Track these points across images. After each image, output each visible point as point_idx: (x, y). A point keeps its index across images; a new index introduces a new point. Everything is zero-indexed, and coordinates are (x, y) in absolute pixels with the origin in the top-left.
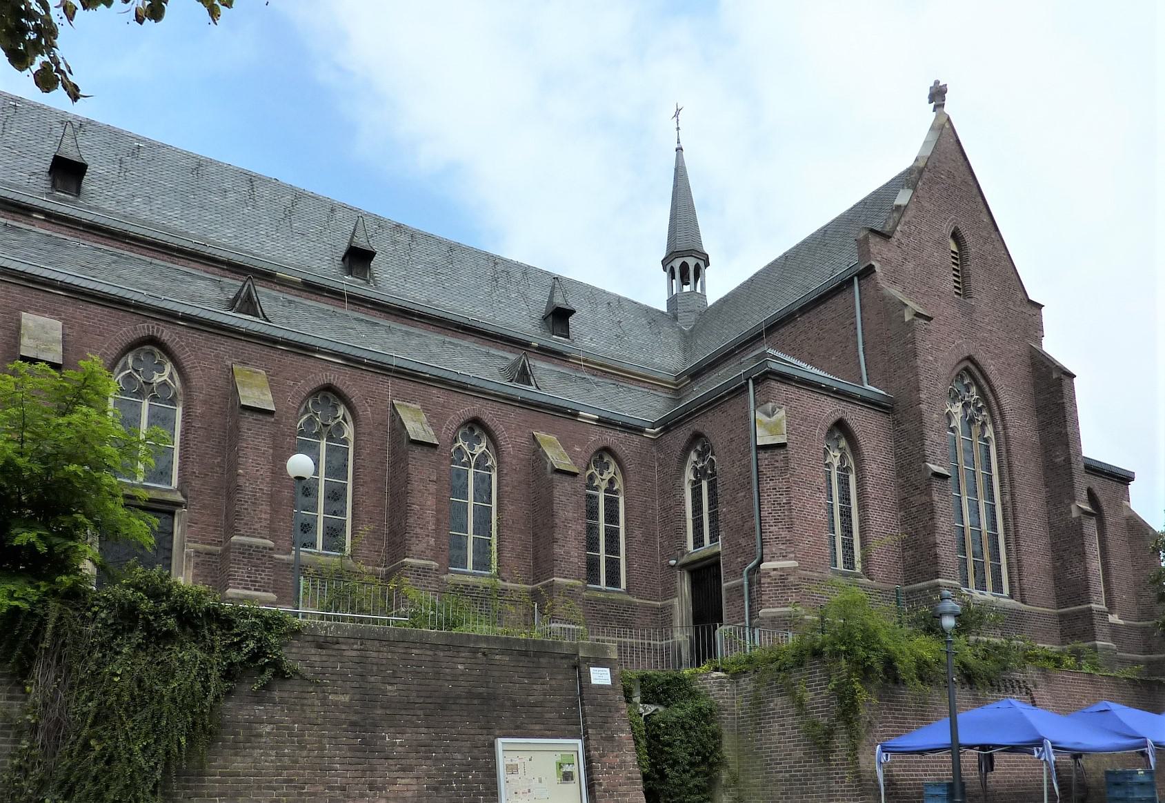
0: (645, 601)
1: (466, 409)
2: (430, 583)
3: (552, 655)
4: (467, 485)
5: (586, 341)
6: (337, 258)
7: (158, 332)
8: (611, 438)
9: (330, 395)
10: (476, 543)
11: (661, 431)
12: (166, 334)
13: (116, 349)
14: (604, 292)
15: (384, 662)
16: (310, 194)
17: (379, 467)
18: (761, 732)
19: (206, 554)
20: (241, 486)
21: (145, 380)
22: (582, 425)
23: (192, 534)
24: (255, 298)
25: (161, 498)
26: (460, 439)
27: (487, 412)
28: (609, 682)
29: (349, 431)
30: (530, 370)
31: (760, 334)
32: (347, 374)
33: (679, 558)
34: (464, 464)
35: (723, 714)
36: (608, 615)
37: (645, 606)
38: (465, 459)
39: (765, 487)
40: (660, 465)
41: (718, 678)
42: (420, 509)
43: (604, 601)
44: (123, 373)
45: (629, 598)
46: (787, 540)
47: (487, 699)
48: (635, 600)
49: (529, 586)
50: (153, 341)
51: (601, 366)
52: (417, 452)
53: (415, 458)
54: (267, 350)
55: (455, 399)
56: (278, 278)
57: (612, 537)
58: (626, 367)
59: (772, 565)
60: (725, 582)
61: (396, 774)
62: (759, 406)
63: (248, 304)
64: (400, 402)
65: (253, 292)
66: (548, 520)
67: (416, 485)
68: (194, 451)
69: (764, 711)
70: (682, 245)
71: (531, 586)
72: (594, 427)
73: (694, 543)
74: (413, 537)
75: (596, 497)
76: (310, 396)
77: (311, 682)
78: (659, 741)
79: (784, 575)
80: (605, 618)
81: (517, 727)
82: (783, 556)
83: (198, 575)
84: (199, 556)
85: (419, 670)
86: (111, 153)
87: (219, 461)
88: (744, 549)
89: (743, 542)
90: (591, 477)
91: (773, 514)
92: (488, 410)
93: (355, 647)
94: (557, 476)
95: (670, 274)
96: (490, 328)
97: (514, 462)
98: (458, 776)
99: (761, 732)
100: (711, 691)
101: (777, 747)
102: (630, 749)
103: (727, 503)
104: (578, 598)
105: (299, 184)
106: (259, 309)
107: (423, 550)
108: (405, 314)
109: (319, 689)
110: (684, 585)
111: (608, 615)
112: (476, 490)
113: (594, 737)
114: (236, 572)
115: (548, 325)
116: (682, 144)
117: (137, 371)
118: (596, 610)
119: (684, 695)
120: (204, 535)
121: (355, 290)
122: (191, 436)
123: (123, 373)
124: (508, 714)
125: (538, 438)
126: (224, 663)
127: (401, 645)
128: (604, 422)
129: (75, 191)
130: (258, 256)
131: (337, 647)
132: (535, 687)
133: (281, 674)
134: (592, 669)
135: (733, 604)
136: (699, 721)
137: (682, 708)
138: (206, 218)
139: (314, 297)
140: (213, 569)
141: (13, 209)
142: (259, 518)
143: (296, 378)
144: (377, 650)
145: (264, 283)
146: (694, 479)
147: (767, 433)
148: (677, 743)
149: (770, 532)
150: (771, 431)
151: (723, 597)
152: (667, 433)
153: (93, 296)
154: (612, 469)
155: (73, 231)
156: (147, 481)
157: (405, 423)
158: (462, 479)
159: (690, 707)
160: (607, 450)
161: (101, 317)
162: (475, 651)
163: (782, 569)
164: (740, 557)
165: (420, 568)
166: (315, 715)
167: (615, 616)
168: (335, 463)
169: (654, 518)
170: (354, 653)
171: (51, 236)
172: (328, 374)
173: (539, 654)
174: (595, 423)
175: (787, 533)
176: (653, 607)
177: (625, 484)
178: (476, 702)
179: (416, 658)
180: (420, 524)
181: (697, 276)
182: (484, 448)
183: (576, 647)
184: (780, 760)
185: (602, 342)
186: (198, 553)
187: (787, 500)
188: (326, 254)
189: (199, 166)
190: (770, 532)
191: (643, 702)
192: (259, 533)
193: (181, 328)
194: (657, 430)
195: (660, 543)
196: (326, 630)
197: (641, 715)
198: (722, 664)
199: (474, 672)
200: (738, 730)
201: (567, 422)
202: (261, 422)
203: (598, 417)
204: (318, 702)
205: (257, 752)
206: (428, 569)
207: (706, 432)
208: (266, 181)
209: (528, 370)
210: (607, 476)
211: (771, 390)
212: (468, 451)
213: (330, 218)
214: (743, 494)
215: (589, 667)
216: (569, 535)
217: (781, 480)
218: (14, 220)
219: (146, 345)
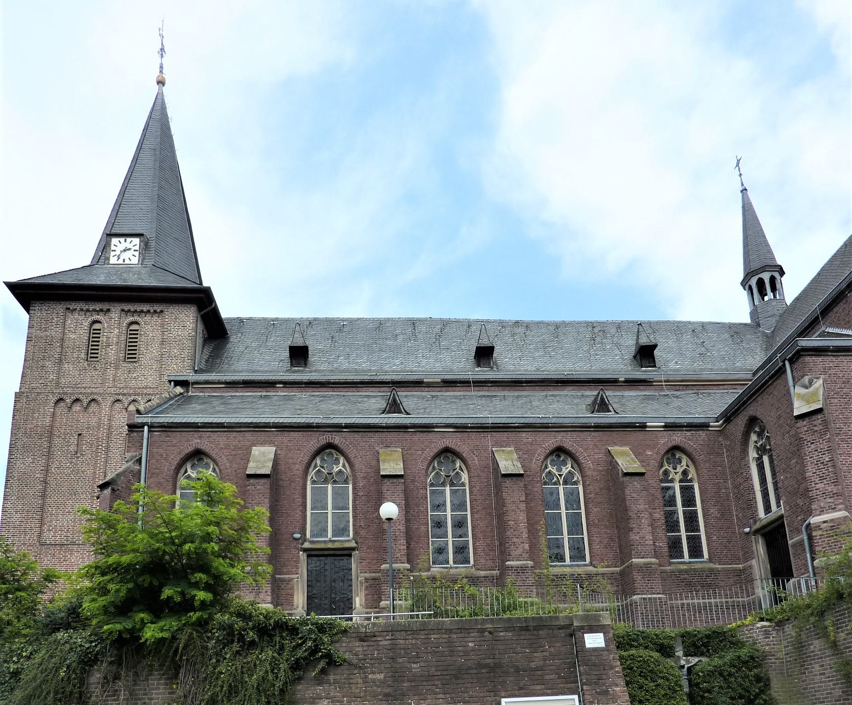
0: (726, 566)
1: (551, 442)
2: (527, 578)
3: (550, 627)
4: (559, 498)
5: (672, 365)
6: (471, 358)
7: (332, 439)
8: (678, 438)
9: (449, 454)
10: (571, 542)
11: (724, 422)
12: (337, 439)
13: (308, 456)
14: (689, 322)
15: (410, 646)
16: (454, 320)
17: (487, 498)
18: (805, 673)
19: (372, 579)
20: (385, 530)
21: (328, 472)
22: (650, 433)
23: (362, 567)
24: (399, 401)
25: (342, 547)
26: (549, 465)
27: (568, 441)
29: (465, 477)
30: (608, 400)
31: (817, 318)
32: (458, 437)
33: (752, 526)
34: (555, 484)
35: (770, 659)
36: (692, 582)
37: (725, 570)
38: (555, 479)
39: (807, 451)
40: (727, 450)
41: (763, 627)
42: (515, 523)
44: (315, 471)
45: (712, 565)
46: (834, 494)
47: (494, 668)
48: (717, 566)
49: (618, 568)
50: (330, 446)
51: (682, 381)
52: (508, 482)
53: (507, 487)
54: (402, 434)
55: (540, 436)
56: (425, 383)
57: (691, 519)
58: (704, 377)
59: (822, 519)
60: (791, 540)
62: (796, 382)
63: (394, 407)
64: (499, 448)
65: (397, 397)
66: (624, 515)
67: (510, 507)
68: (360, 512)
69: (806, 653)
70: (755, 266)
71: (619, 568)
72: (662, 432)
73: (765, 511)
74: (511, 545)
75: (673, 488)
76: (434, 459)
77: (356, 667)
78: (700, 688)
79: (835, 525)
81: (521, 689)
82: (832, 509)
83: (368, 595)
84: (367, 582)
85: (436, 650)
86: (327, 334)
87: (376, 515)
88: (802, 509)
89: (800, 502)
90: (666, 473)
91: (818, 473)
92: (568, 439)
93: (388, 637)
94: (627, 478)
95: (750, 291)
96: (582, 377)
97: (595, 474)
99: (805, 673)
100: (757, 640)
101: (819, 687)
102: (624, 701)
103: (784, 471)
104: (655, 572)
105: (445, 316)
106: (402, 408)
107: (520, 553)
108: (516, 384)
109: (361, 671)
110: (760, 548)
111: (692, 582)
112: (567, 501)
113: (588, 693)
114: (385, 589)
115: (637, 362)
116: (746, 185)
117: (322, 467)
118: (680, 579)
119: (725, 646)
120: (371, 567)
121: (478, 377)
122: (357, 502)
123: (315, 471)
124: (511, 679)
125: (612, 452)
126: (293, 659)
127: (423, 632)
128: (670, 427)
129: (303, 363)
130: (415, 372)
131: (374, 639)
132: (536, 655)
133: (332, 662)
134: (586, 635)
135: (799, 558)
136: (740, 669)
137: (721, 657)
138: (383, 357)
139: (451, 389)
140: (377, 589)
141: (268, 385)
142: (399, 550)
143: (423, 449)
144: (404, 638)
145: (403, 389)
146: (757, 456)
147: (803, 403)
148: (716, 689)
149: (816, 489)
150: (807, 400)
151: (790, 553)
152: (729, 423)
153: (292, 427)
154: (684, 463)
155: (300, 389)
156: (335, 537)
157: (499, 463)
158: (555, 495)
159: (729, 656)
160: (676, 448)
161: (298, 439)
162: (482, 631)
163: (832, 520)
164: (800, 515)
165: (519, 568)
166: (357, 691)
167: (699, 581)
168: (456, 502)
169: (728, 495)
171: (286, 395)
172: (445, 441)
173: (538, 628)
174: (663, 429)
175: (833, 487)
176: (735, 570)
177: (698, 475)
178: (484, 671)
179: (435, 641)
180: (515, 535)
181: (774, 289)
182: (570, 468)
183: (571, 619)
184: (823, 698)
185: (686, 363)
186: (366, 579)
187: (829, 458)
188: (463, 357)
189: (380, 325)
190: (816, 489)
191: (686, 655)
192: (400, 560)
193: (346, 434)
194: (721, 422)
195: (736, 515)
196: (366, 628)
197: (683, 667)
198: (767, 614)
199: (482, 648)
200: (788, 673)
201: (638, 433)
202: (395, 484)
203: (664, 424)
204: (360, 681)
206: (525, 567)
207: (758, 415)
208: (420, 320)
209: (606, 400)
210: (680, 469)
211: (806, 365)
213: (467, 332)
214: (795, 460)
215: (583, 633)
216: (642, 523)
217: (821, 442)
218: (267, 392)
219: (326, 449)
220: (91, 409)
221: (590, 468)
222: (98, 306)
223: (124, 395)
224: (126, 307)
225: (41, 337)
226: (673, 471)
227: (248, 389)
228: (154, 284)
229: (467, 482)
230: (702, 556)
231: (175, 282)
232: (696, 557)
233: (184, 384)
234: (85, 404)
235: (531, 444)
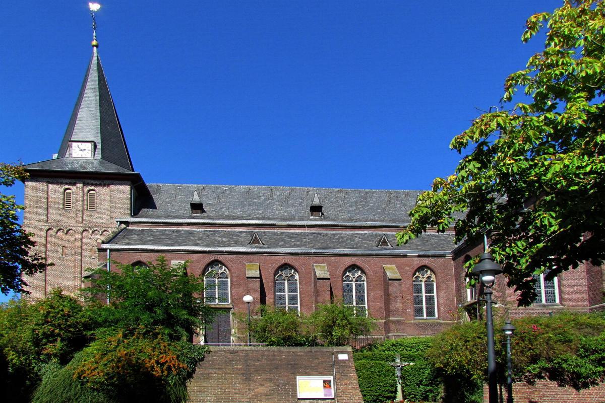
8: (426, 261)
29: (297, 277)
34: (350, 281)
38: (351, 279)
45: (439, 321)
75: (421, 285)
81: (306, 373)
94: (391, 281)
158: (350, 286)
177: (436, 279)
205: (211, 381)
210: (426, 276)
221: (371, 275)
227: (166, 226)
228: (103, 170)
229: (298, 279)
231: (116, 169)
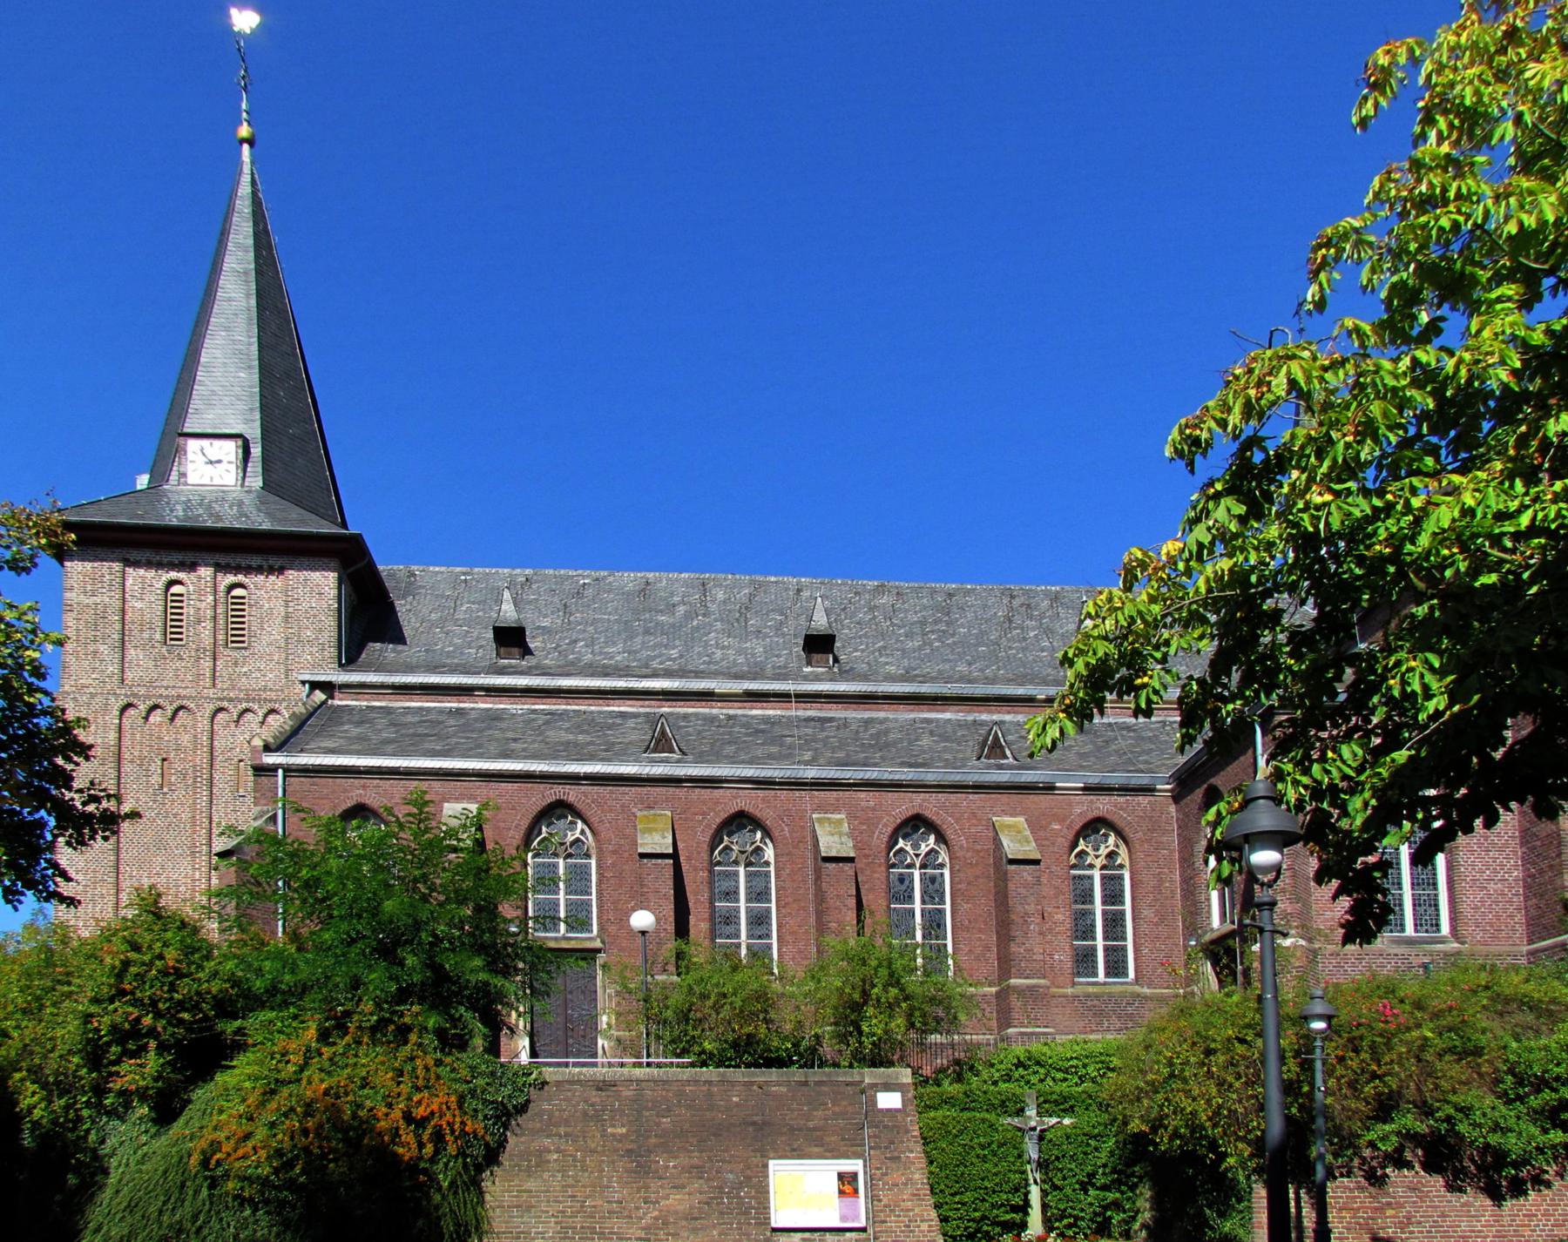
8: (1103, 805)
12: (571, 794)
28: (899, 1105)
29: (769, 853)
43: (1097, 996)
55: (890, 797)
57: (1114, 924)
61: (667, 1191)
75: (1091, 878)
80: (1100, 1014)
81: (794, 1150)
94: (1013, 867)
98: (728, 1193)
125: (997, 825)
158: (907, 882)
170: (631, 1093)
205: (546, 1175)
210: (1103, 851)
212: (911, 852)
220: (178, 721)
221: (961, 847)
222: (176, 557)
223: (230, 700)
224: (223, 560)
225: (88, 606)
226: (1092, 853)
228: (265, 527)
229: (772, 861)
230: (1126, 975)
231: (303, 522)
232: (1116, 975)
233: (327, 687)
234: (169, 713)
235: (874, 809)
